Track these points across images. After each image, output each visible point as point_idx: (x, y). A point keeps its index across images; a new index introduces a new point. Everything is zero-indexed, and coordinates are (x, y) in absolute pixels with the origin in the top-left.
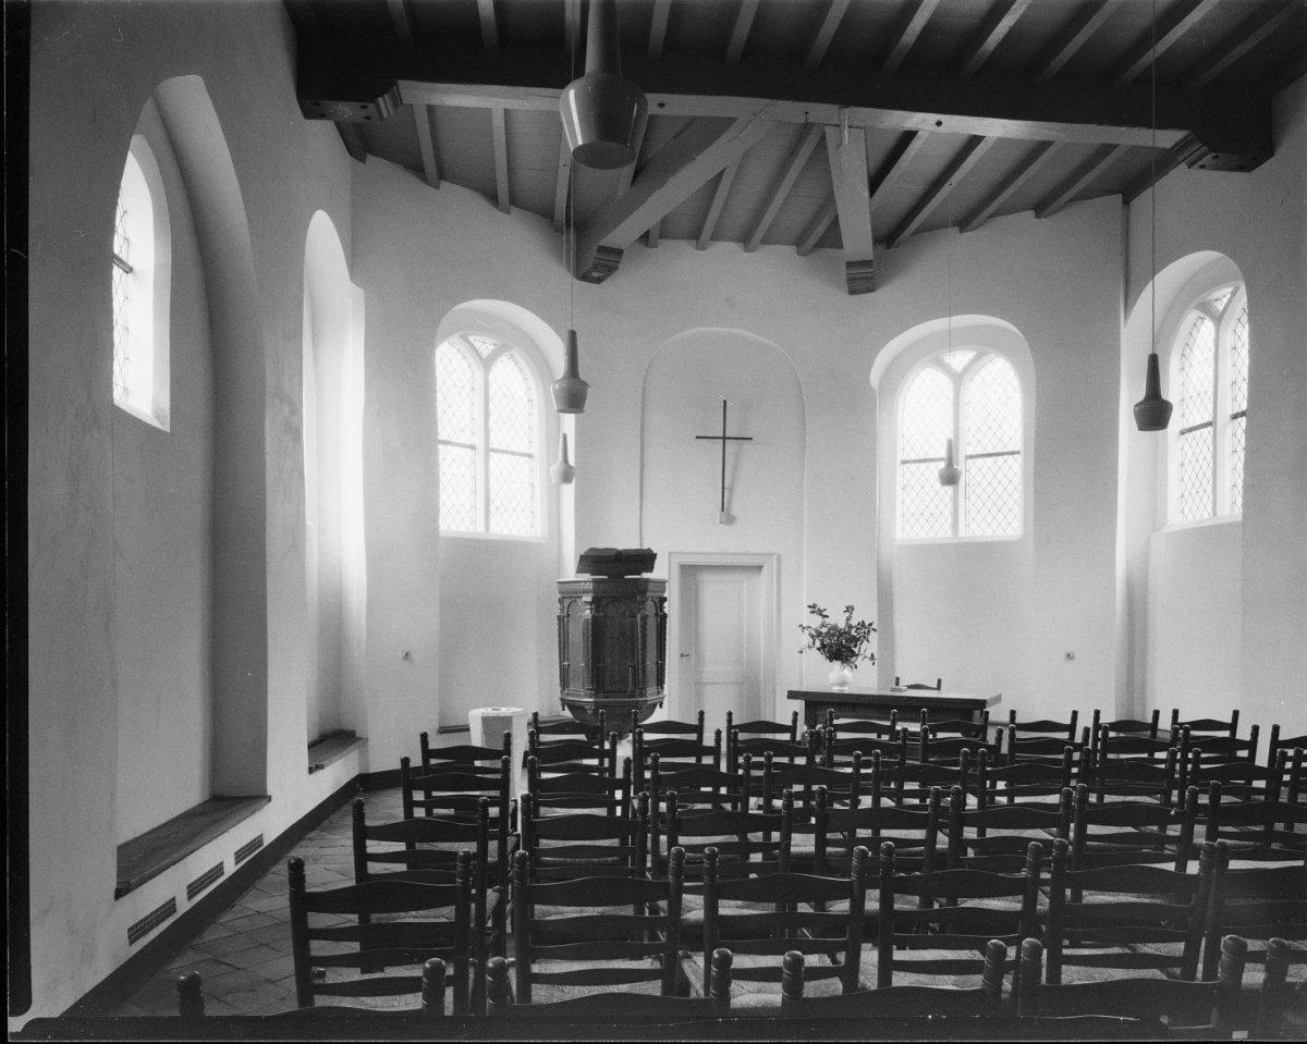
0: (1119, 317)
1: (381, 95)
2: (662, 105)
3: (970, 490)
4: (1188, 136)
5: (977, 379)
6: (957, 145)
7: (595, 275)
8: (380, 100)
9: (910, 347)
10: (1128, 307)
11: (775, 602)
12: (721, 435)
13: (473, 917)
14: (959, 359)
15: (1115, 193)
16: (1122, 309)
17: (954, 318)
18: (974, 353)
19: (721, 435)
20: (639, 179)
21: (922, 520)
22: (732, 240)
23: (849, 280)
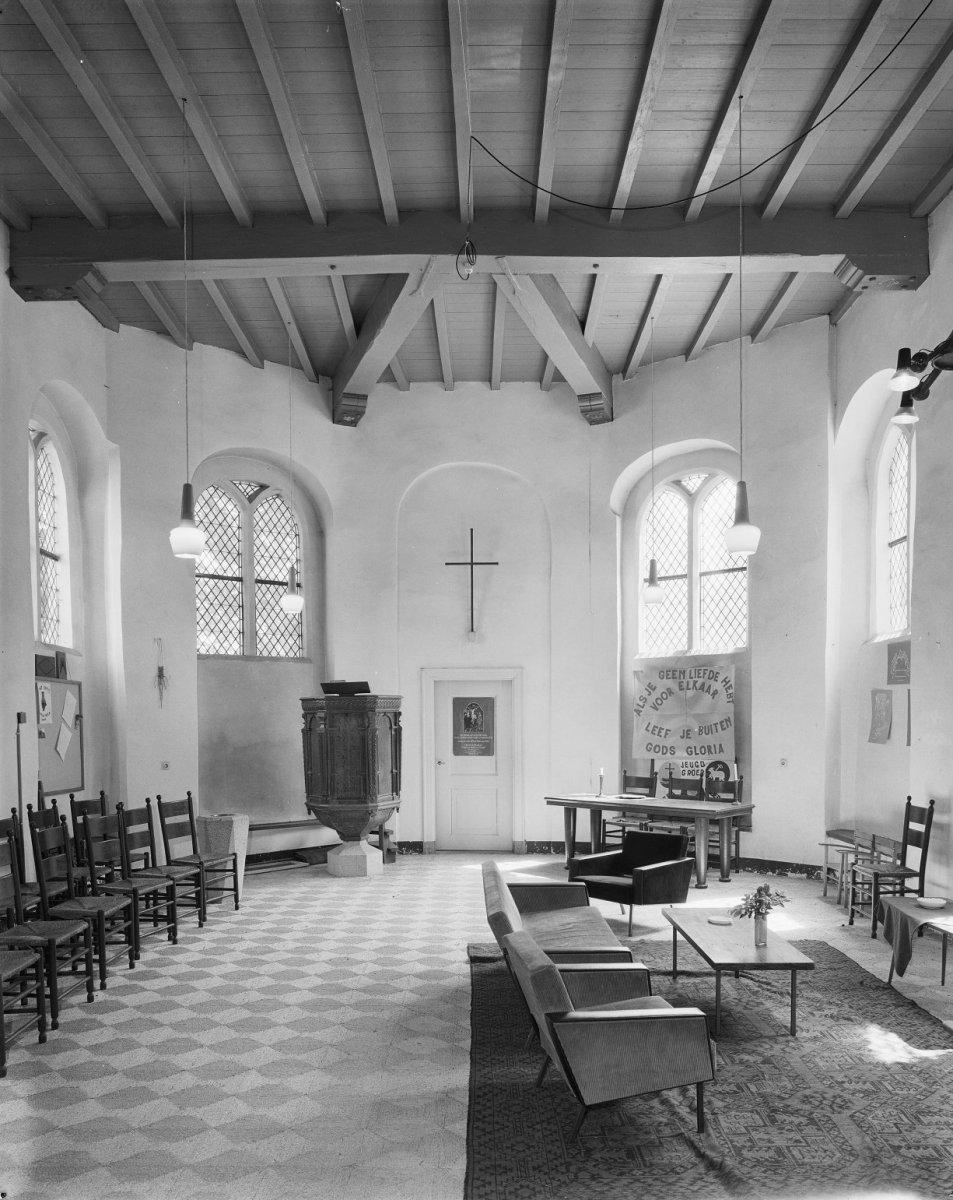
0: (826, 436)
1: (859, 268)
2: (596, 266)
3: (704, 606)
4: (844, 260)
5: (711, 499)
6: (722, 278)
7: (348, 419)
8: (854, 269)
9: (653, 469)
10: (837, 419)
11: (425, 763)
12: (469, 561)
13: (229, 1058)
14: (693, 482)
15: (824, 314)
16: (829, 421)
17: (656, 450)
18: (703, 476)
19: (470, 566)
20: (362, 332)
21: (663, 635)
22: (474, 380)
23: (582, 412)
